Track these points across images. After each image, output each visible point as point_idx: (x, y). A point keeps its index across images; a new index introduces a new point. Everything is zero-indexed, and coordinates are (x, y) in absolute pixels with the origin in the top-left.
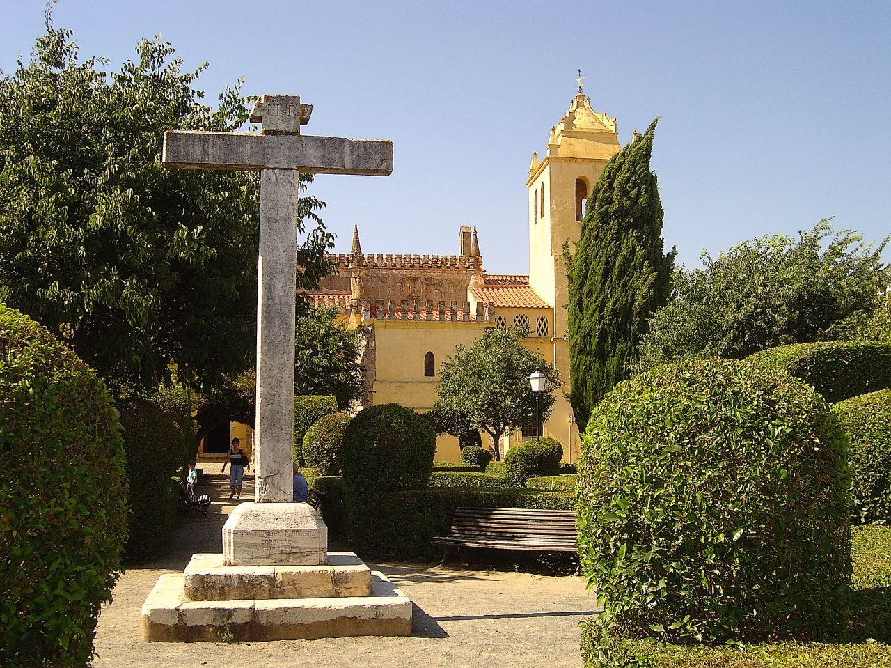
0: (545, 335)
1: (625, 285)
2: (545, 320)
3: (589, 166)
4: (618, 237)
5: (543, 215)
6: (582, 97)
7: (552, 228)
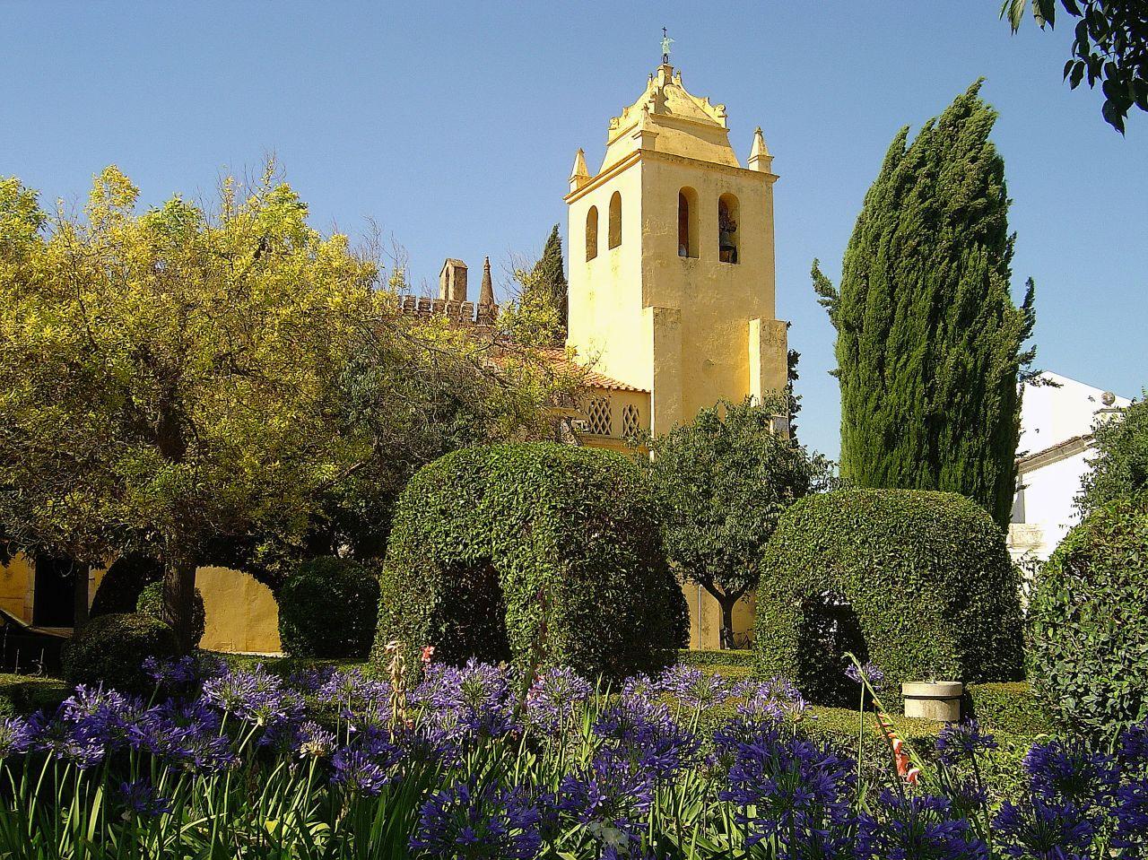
0: (607, 433)
1: (972, 339)
2: (635, 412)
3: (700, 172)
4: (954, 251)
5: (615, 241)
6: (669, 70)
7: (645, 263)
